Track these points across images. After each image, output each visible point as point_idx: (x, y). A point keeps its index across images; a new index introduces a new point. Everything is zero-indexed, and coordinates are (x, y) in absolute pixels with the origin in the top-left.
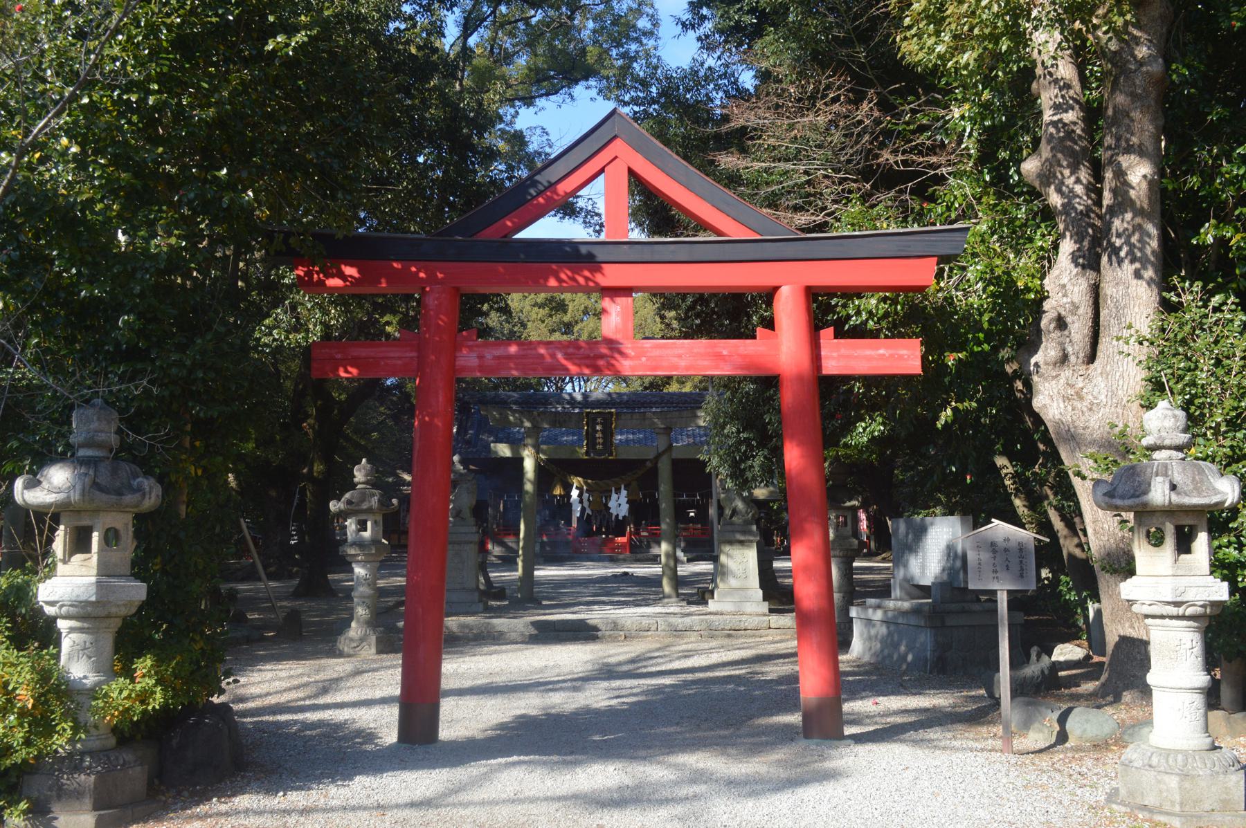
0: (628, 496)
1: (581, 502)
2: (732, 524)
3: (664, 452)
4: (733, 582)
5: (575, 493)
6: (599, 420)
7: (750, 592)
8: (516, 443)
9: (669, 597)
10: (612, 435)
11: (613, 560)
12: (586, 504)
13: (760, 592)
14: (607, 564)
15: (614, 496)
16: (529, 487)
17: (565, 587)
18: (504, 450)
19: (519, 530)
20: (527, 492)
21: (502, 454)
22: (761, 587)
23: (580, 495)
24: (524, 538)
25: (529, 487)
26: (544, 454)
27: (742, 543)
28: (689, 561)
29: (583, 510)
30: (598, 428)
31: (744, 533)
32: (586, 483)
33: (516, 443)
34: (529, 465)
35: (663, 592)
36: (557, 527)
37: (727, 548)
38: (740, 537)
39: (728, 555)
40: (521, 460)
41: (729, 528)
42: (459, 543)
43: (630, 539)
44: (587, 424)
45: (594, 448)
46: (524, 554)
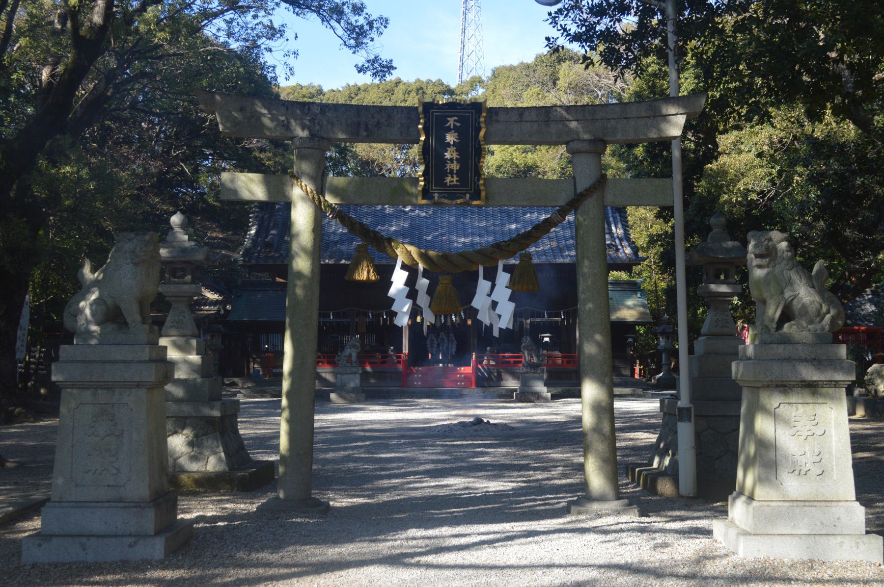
0: (511, 285)
1: (412, 294)
2: (787, 341)
3: (589, 192)
4: (793, 486)
5: (399, 278)
6: (451, 121)
7: (838, 511)
8: (278, 176)
9: (601, 499)
10: (479, 153)
11: (456, 396)
12: (423, 300)
13: (859, 513)
14: (447, 402)
15: (483, 285)
16: (302, 264)
17: (388, 448)
18: (251, 187)
19: (281, 354)
20: (299, 275)
21: (246, 195)
22: (861, 497)
23: (411, 282)
24: (292, 373)
25: (302, 264)
26: (335, 192)
27: (812, 388)
28: (555, 397)
29: (415, 311)
30: (450, 138)
31: (818, 363)
32: (424, 257)
33: (278, 176)
34: (302, 217)
35: (584, 486)
36: (385, 355)
37: (774, 401)
38: (810, 374)
39: (776, 417)
40: (288, 206)
41: (780, 350)
42: (109, 387)
43: (476, 369)
44: (426, 129)
45: (441, 183)
46: (291, 406)
